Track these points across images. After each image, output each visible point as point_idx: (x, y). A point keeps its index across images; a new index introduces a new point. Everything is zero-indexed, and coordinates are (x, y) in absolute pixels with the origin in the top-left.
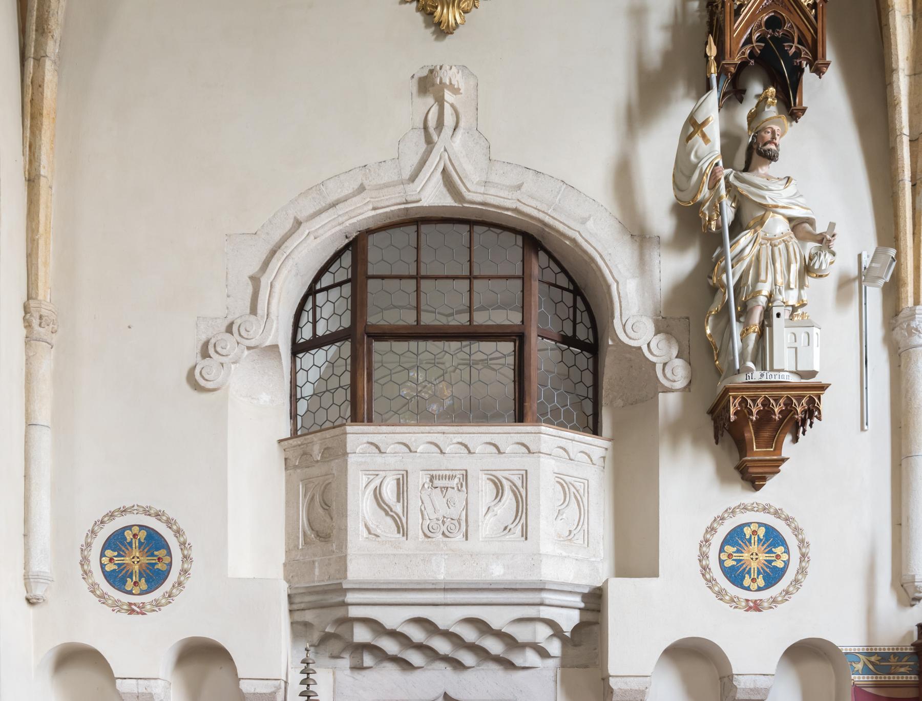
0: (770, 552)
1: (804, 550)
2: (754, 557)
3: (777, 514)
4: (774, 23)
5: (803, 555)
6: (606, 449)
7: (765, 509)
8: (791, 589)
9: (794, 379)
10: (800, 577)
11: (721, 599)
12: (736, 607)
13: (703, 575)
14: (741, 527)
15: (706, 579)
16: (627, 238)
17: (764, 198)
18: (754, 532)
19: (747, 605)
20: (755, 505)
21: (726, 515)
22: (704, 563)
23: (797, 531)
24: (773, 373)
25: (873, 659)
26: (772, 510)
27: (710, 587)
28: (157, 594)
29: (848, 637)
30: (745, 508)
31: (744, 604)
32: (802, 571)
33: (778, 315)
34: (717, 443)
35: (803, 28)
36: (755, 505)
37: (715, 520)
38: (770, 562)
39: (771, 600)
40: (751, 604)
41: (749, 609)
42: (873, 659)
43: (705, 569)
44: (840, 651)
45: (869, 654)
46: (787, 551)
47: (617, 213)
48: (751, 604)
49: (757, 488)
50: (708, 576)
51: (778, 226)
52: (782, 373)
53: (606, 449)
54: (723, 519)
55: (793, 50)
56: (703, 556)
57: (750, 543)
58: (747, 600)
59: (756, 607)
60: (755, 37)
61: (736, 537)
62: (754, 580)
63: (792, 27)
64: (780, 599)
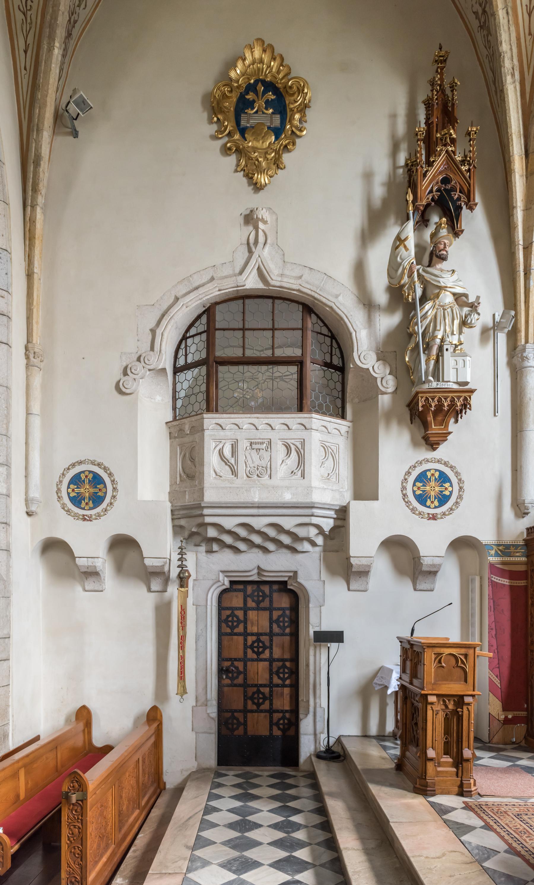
0: (442, 486)
1: (461, 485)
2: (433, 489)
3: (446, 464)
4: (446, 181)
5: (461, 488)
6: (349, 427)
7: (439, 461)
8: (454, 507)
9: (455, 387)
10: (459, 500)
11: (414, 513)
12: (422, 518)
13: (404, 499)
14: (426, 471)
15: (405, 502)
16: (361, 306)
17: (439, 282)
18: (433, 475)
19: (429, 516)
20: (433, 459)
21: (417, 465)
22: (404, 492)
23: (457, 474)
24: (444, 383)
25: (501, 548)
26: (443, 462)
27: (407, 506)
28: (99, 510)
29: (486, 535)
30: (428, 461)
31: (426, 516)
32: (460, 497)
33: (447, 350)
34: (412, 423)
35: (462, 183)
36: (433, 459)
37: (410, 468)
38: (442, 492)
39: (442, 514)
40: (431, 516)
41: (430, 519)
42: (501, 548)
43: (405, 496)
44: (482, 543)
45: (498, 545)
46: (451, 486)
47: (356, 292)
48: (431, 516)
49: (434, 449)
50: (406, 500)
51: (447, 298)
52: (449, 383)
53: (349, 427)
54: (415, 467)
55: (457, 196)
56: (404, 488)
57: (430, 481)
58: (429, 514)
59: (434, 517)
60: (435, 189)
61: (422, 478)
62: (432, 502)
63: (456, 183)
64: (447, 513)
